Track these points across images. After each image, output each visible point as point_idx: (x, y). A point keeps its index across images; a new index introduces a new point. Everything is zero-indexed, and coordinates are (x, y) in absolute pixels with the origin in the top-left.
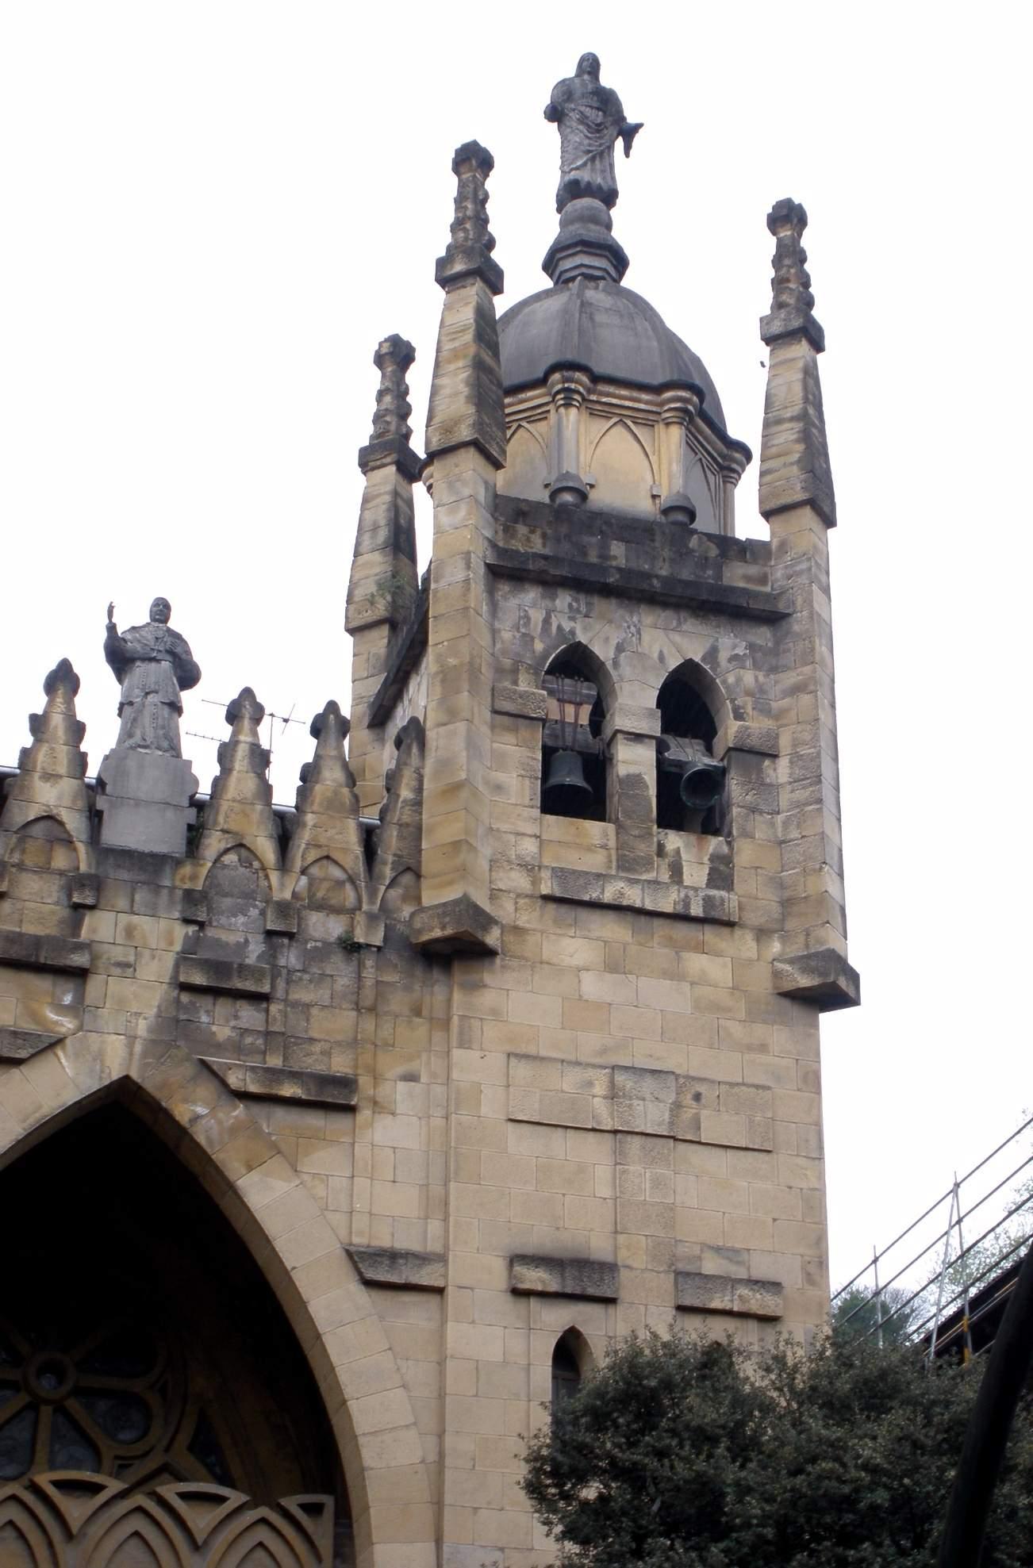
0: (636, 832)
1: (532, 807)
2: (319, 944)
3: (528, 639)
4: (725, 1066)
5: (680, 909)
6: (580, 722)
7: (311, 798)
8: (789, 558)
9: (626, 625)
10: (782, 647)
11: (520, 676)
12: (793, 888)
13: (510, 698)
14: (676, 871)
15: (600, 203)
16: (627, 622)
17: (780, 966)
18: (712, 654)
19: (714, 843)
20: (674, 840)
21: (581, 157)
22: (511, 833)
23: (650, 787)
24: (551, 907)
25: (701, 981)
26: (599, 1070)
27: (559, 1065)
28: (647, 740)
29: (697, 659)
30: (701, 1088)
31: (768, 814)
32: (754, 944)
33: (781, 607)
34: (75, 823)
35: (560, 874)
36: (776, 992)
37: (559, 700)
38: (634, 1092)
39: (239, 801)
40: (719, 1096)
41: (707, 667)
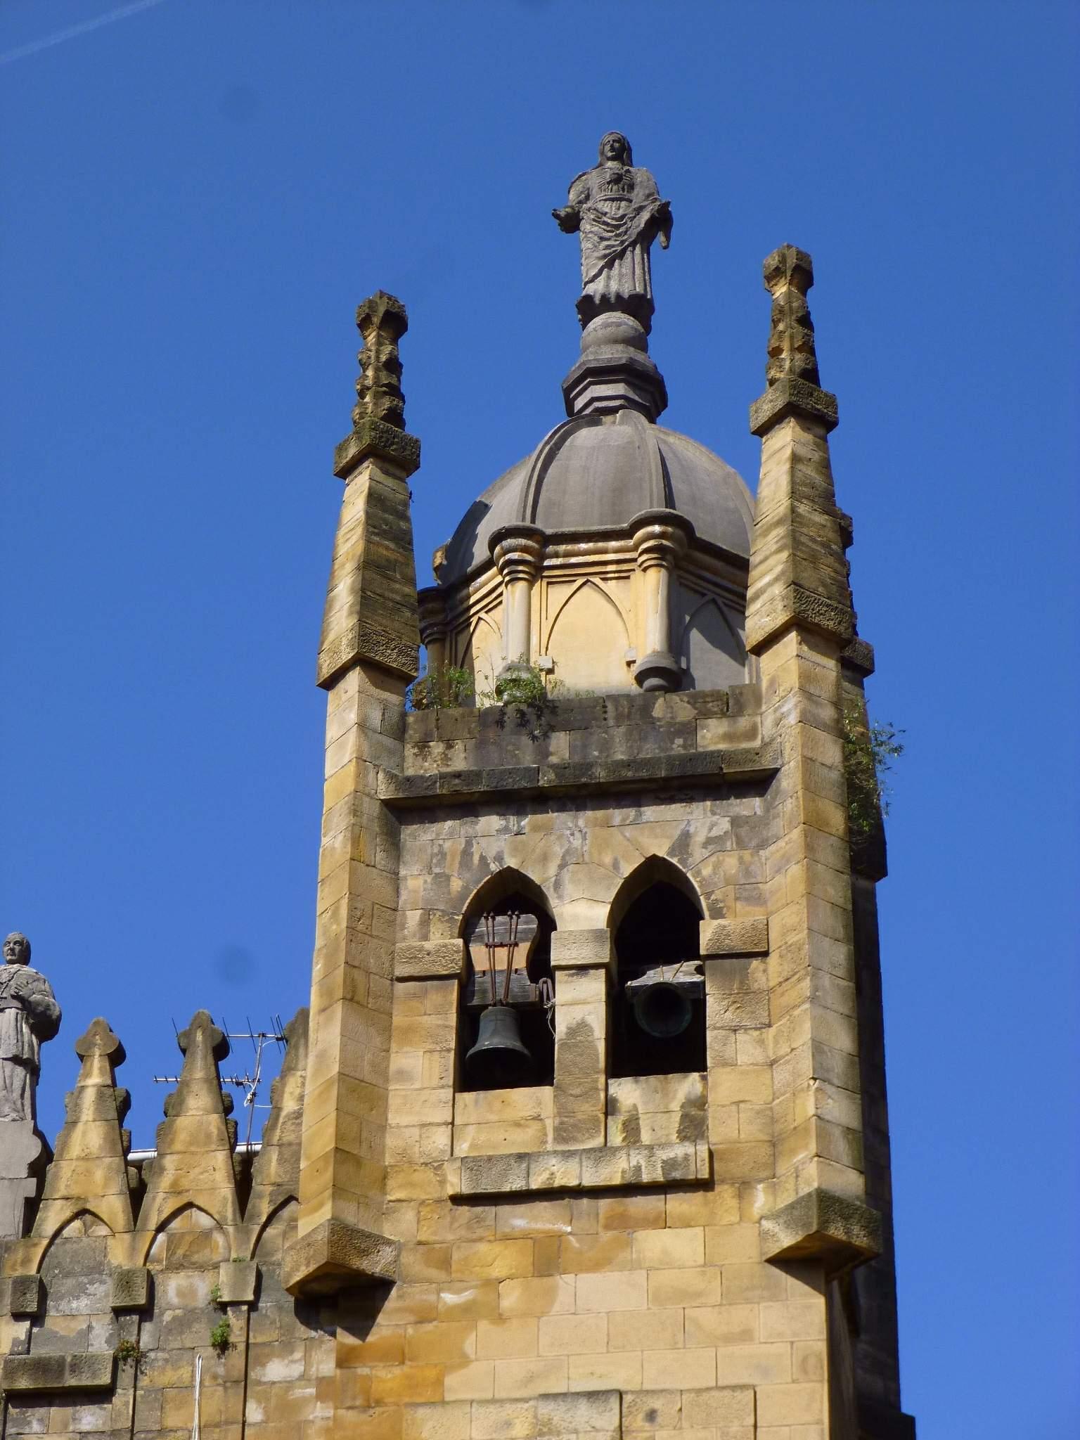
0: (577, 1091)
1: (443, 1087)
2: (178, 1312)
5: (630, 1178)
6: (514, 967)
7: (171, 1136)
8: (778, 699)
9: (568, 832)
10: (772, 812)
11: (432, 930)
12: (783, 1120)
13: (416, 957)
14: (632, 1129)
15: (623, 315)
16: (570, 829)
17: (767, 1224)
20: (628, 1091)
21: (595, 265)
22: (414, 1126)
24: (464, 1210)
25: (667, 1263)
26: (519, 1405)
27: (467, 1409)
28: (592, 972)
29: (662, 853)
30: (657, 1403)
31: (756, 1029)
32: (734, 1203)
33: (766, 763)
35: (472, 1164)
36: (765, 1258)
37: (487, 946)
38: (565, 1424)
39: (83, 1159)
40: (680, 1410)
41: (674, 861)
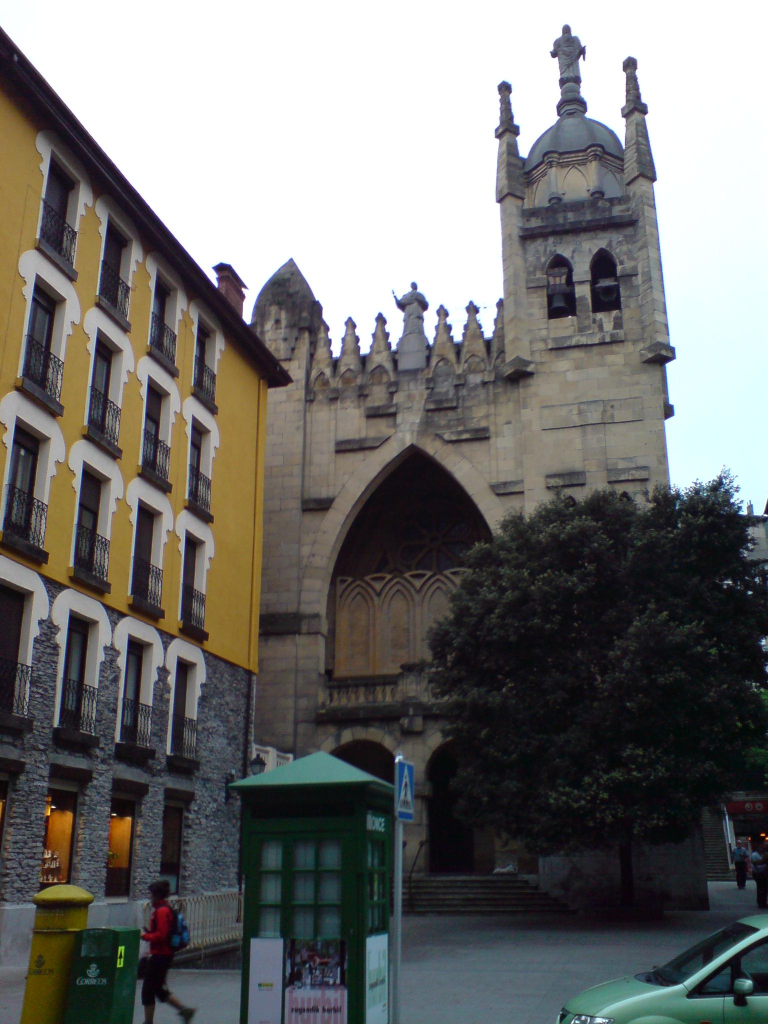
3: (539, 259)
18: (610, 244)
19: (615, 313)
30: (612, 403)
41: (608, 249)
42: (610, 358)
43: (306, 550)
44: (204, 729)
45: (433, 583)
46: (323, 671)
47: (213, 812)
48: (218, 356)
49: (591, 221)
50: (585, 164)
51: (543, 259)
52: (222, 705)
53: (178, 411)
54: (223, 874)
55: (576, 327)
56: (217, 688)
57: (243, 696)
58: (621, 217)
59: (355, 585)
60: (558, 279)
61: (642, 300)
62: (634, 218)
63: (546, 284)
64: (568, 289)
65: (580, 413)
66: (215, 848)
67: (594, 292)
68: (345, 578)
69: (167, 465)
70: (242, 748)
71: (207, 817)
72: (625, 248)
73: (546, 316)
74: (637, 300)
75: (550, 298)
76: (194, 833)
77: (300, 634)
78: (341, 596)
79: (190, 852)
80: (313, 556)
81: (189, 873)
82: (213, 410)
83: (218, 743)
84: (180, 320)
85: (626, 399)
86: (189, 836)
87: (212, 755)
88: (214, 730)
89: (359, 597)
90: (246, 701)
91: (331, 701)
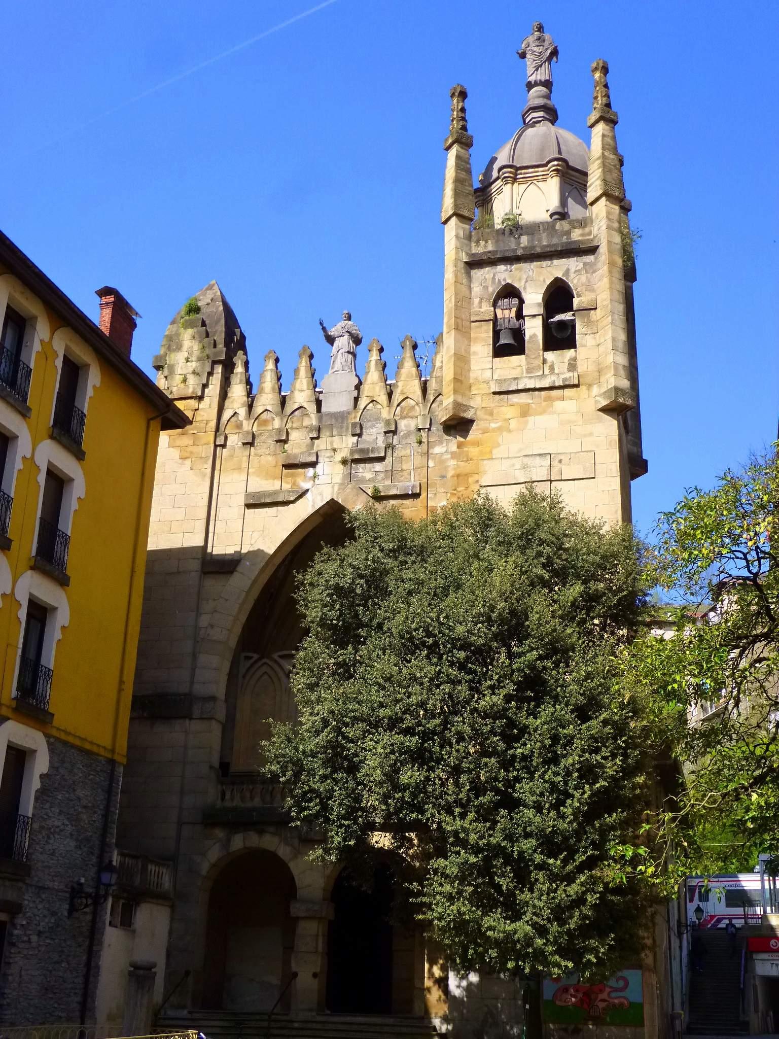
3: (486, 288)
4: (571, 446)
5: (551, 385)
17: (597, 398)
18: (567, 272)
19: (570, 353)
23: (42, 471)
24: (497, 396)
29: (560, 276)
30: (562, 457)
34: (312, 408)
35: (500, 382)
41: (564, 278)
42: (559, 405)
43: (204, 620)
44: (42, 827)
45: (260, 667)
46: (216, 764)
47: (49, 928)
48: (90, 392)
49: (547, 246)
50: (545, 180)
51: (490, 289)
52: (72, 800)
53: (28, 456)
54: (59, 1004)
55: (524, 368)
56: (65, 780)
57: (103, 790)
58: (579, 241)
59: (260, 663)
60: (507, 312)
61: (600, 338)
62: (595, 244)
63: (492, 317)
64: (515, 323)
65: (525, 467)
66: (51, 971)
67: (546, 327)
68: (250, 654)
69: (8, 517)
70: (97, 852)
71: (40, 934)
72: (583, 278)
73: (491, 354)
74: (595, 338)
75: (496, 334)
76: (19, 952)
77: (191, 719)
78: (244, 677)
79: (12, 975)
80: (212, 626)
81: (8, 1000)
82: (79, 455)
83: (64, 845)
84: (38, 352)
85: (576, 453)
86: (12, 956)
87: (52, 859)
88: (57, 830)
89: (266, 677)
90: (107, 796)
91: (223, 799)
